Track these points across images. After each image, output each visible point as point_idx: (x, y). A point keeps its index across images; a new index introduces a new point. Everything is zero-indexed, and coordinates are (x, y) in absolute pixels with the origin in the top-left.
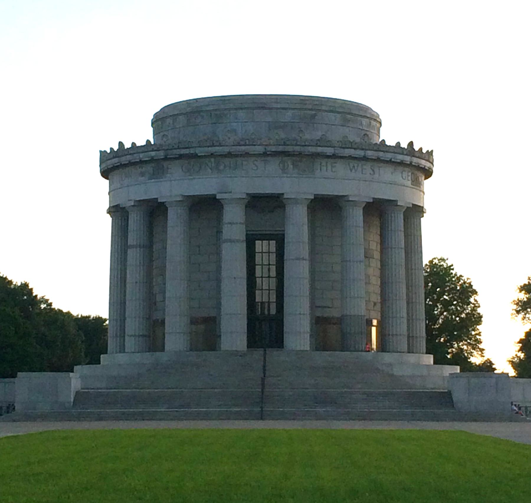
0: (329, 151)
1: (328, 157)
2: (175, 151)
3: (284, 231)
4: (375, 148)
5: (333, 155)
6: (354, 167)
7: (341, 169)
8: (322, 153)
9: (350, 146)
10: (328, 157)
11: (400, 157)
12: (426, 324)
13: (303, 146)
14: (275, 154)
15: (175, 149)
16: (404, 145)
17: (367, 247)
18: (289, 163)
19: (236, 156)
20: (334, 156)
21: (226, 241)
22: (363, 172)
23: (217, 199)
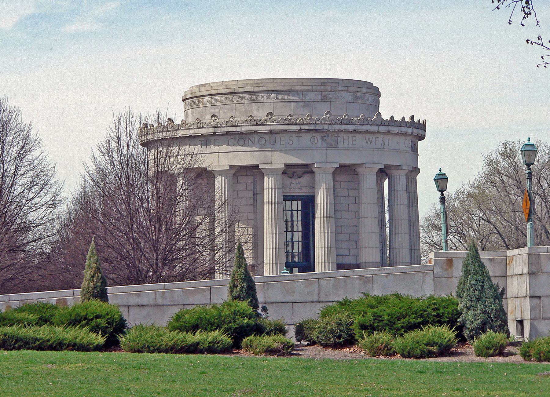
0: (351, 128)
2: (223, 128)
5: (406, 133)
6: (369, 139)
9: (367, 123)
10: (351, 132)
11: (404, 130)
12: (308, 345)
13: (331, 124)
15: (223, 127)
19: (276, 133)
20: (355, 131)
22: (353, 143)
23: (260, 169)
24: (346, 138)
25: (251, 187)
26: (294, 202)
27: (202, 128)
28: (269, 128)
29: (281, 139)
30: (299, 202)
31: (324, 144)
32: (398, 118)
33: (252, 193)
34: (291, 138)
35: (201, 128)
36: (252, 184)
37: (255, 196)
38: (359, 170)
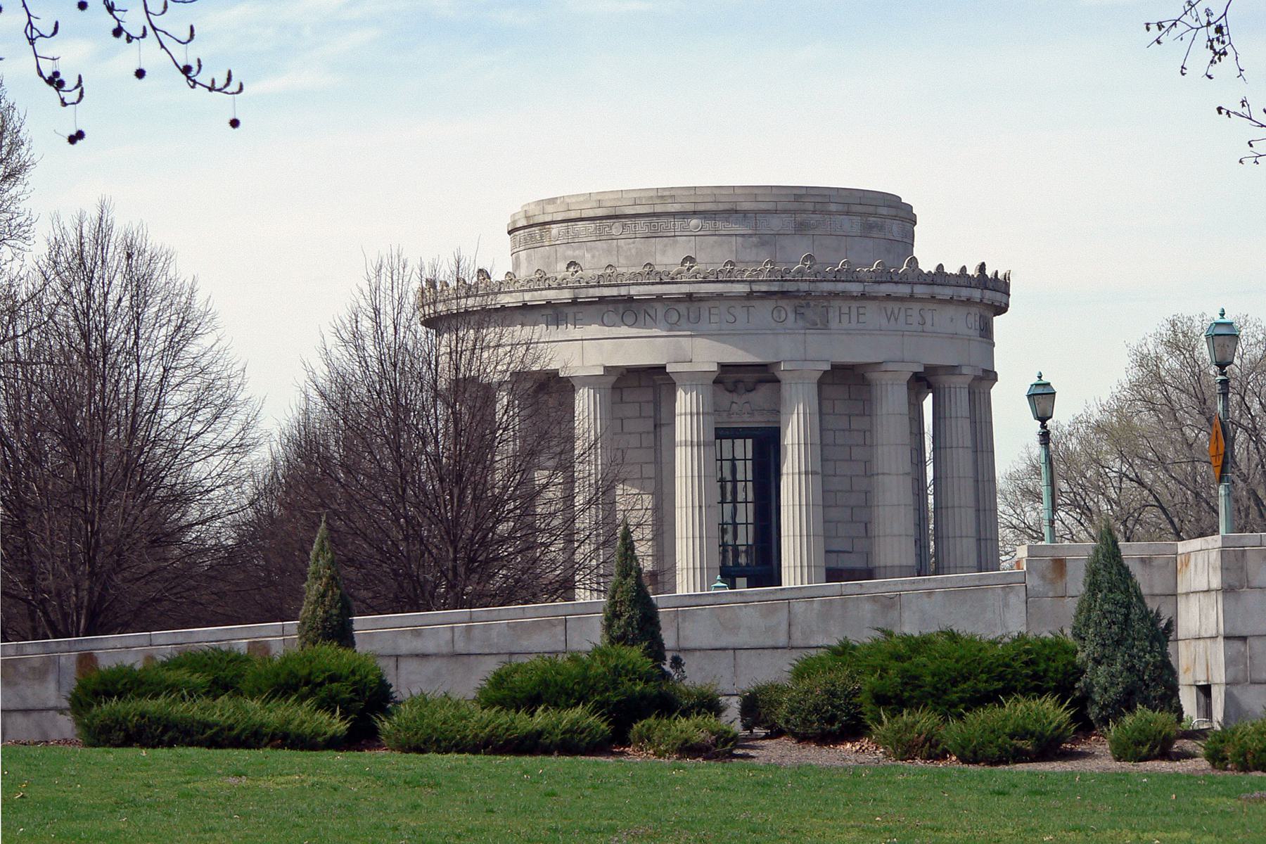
0: (855, 288)
1: (854, 298)
3: (779, 422)
4: (929, 281)
6: (892, 312)
7: (873, 315)
8: (843, 292)
10: (854, 298)
11: (965, 293)
14: (768, 295)
16: (972, 271)
17: (129, 252)
18: (789, 310)
20: (863, 296)
21: (910, 505)
23: (668, 373)
24: (845, 310)
25: (649, 410)
26: (739, 442)
27: (549, 289)
28: (686, 289)
29: (712, 312)
30: (749, 442)
31: (801, 323)
32: (952, 268)
33: (651, 423)
34: (732, 310)
35: (546, 289)
36: (652, 405)
37: (658, 430)
38: (873, 376)
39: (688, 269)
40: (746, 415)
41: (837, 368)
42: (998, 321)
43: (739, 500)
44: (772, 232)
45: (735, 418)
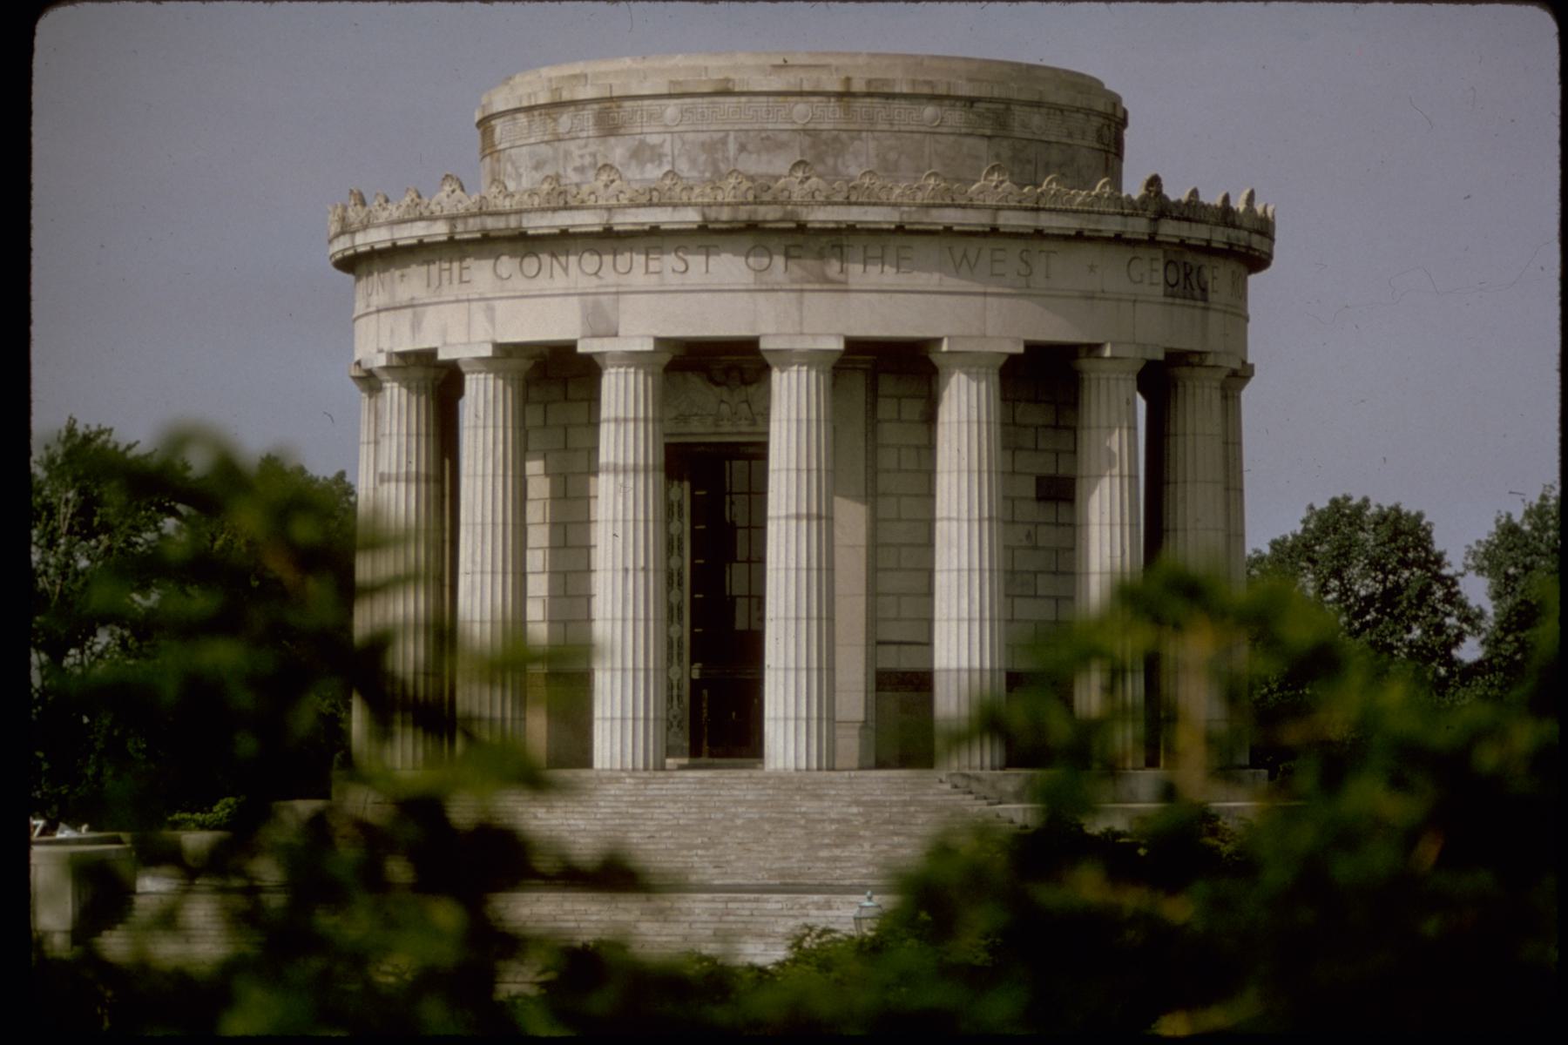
39: (606, 186)
40: (743, 422)
41: (855, 346)
42: (1254, 280)
43: (739, 558)
44: (795, 127)
45: (726, 427)
